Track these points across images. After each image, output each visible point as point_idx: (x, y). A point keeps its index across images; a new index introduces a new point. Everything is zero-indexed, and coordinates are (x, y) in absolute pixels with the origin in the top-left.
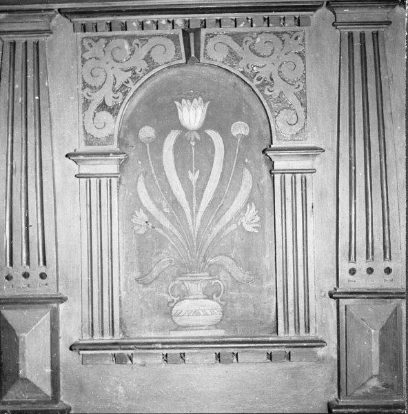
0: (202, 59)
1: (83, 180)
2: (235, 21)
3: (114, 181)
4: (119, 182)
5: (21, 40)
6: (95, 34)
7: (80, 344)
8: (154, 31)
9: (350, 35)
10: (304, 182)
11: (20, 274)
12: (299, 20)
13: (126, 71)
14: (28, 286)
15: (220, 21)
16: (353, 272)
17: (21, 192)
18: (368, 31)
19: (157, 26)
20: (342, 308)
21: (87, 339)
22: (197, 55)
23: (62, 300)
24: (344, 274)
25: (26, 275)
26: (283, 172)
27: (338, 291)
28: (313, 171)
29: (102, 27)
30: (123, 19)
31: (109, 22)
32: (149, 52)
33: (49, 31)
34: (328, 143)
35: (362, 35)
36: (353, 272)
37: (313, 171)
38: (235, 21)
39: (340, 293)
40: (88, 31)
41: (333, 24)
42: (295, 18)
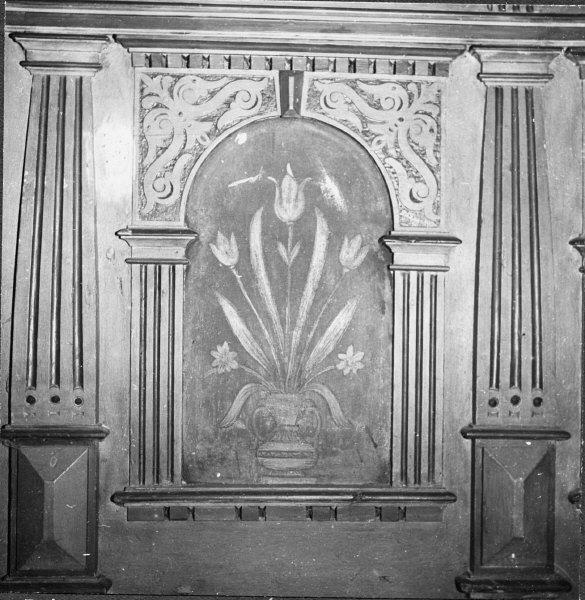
0: (304, 112)
1: (136, 267)
2: (229, 60)
3: (180, 268)
4: (187, 271)
5: (72, 75)
6: (205, 71)
7: (125, 494)
8: (329, 74)
9: (499, 91)
10: (434, 279)
11: (47, 399)
12: (434, 68)
13: (204, 120)
14: (59, 413)
15: (188, 59)
16: (493, 403)
17: (36, 189)
18: (522, 85)
19: (188, 63)
20: (479, 451)
21: (136, 487)
22: (297, 106)
23: (21, 63)
24: (482, 404)
25: (55, 400)
26: (407, 270)
27: (475, 428)
28: (445, 269)
29: (422, 68)
30: (206, 52)
31: (186, 56)
32: (438, 139)
33: (550, 76)
34: (468, 235)
35: (64, 81)
36: (493, 403)
37: (445, 269)
38: (229, 60)
39: (477, 431)
40: (400, 72)
41: (478, 75)
42: (391, 64)
